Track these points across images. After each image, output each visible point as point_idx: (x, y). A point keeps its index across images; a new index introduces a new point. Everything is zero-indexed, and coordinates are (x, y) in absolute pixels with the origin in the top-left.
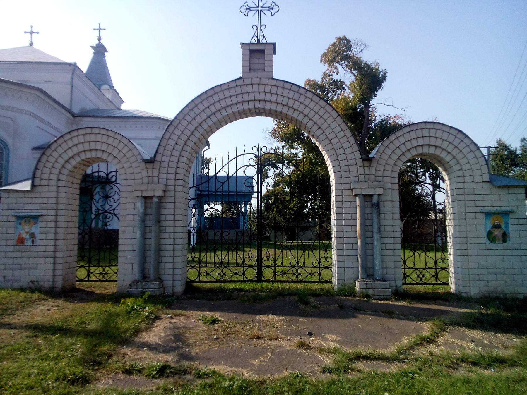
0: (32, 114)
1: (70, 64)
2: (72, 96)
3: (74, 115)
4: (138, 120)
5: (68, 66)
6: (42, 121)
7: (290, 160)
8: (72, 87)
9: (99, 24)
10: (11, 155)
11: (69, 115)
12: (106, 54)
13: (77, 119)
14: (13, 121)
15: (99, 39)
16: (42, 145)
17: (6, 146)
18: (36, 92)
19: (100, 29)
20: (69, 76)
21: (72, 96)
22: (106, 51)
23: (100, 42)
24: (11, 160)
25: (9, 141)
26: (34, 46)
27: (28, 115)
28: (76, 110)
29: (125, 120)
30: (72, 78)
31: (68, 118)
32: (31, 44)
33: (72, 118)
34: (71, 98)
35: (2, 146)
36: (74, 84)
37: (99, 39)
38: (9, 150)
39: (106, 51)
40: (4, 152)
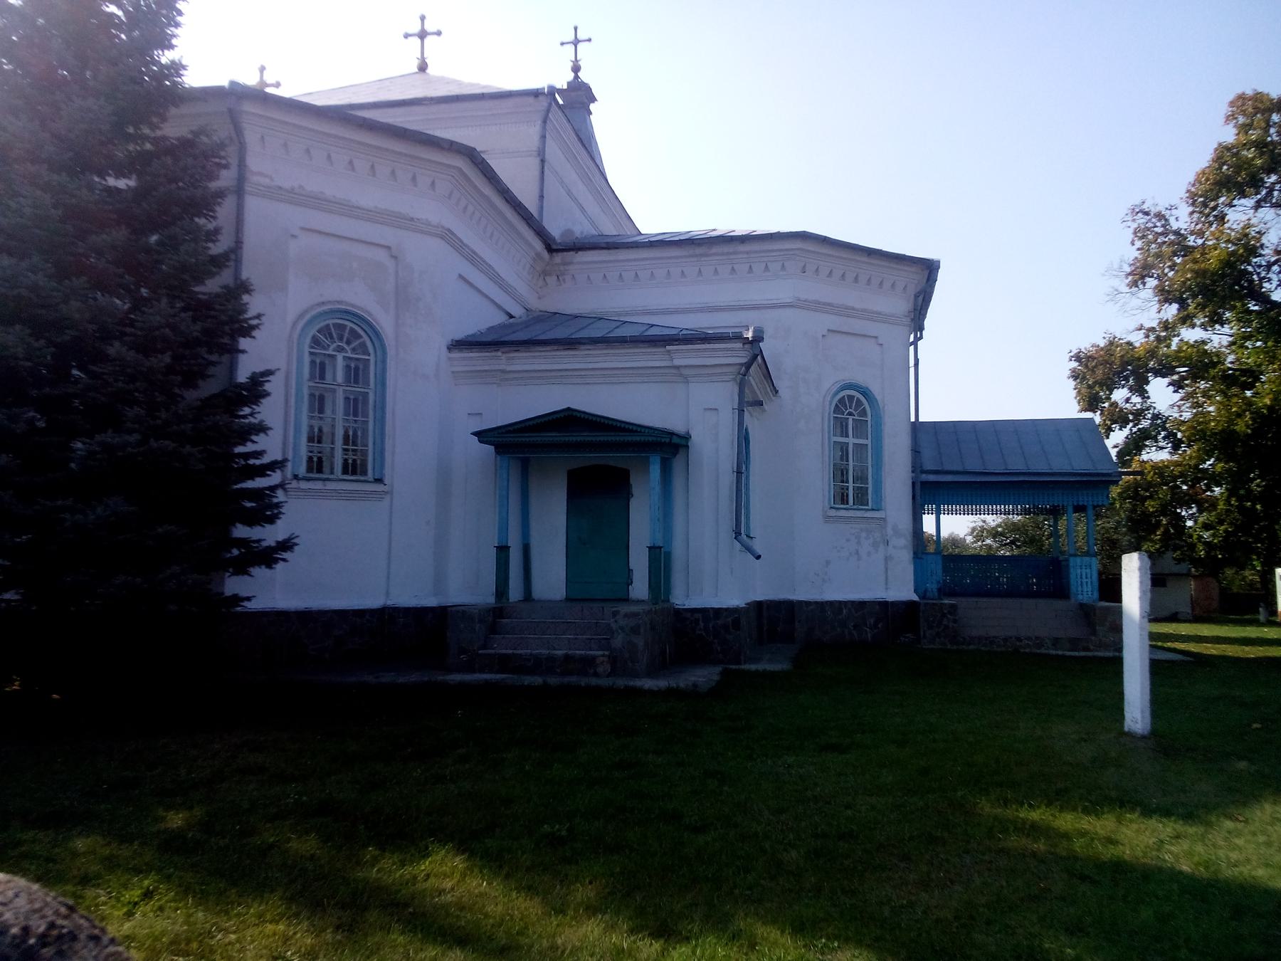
0: (448, 236)
1: (536, 94)
2: (542, 190)
3: (552, 247)
4: (742, 248)
5: (531, 100)
6: (473, 258)
7: (1200, 365)
8: (543, 161)
9: (576, 29)
10: (391, 363)
11: (538, 245)
12: (592, 107)
13: (558, 258)
14: (395, 258)
15: (576, 69)
16: (473, 335)
17: (376, 334)
18: (460, 162)
19: (576, 42)
20: (534, 131)
21: (542, 190)
22: (593, 99)
23: (577, 77)
24: (390, 382)
25: (385, 322)
26: (428, 71)
27: (436, 235)
28: (555, 229)
29: (699, 251)
30: (543, 137)
31: (538, 255)
32: (423, 67)
33: (546, 254)
34: (542, 197)
35: (365, 338)
36: (547, 157)
37: (576, 69)
38: (384, 353)
39: (593, 99)
40: (372, 358)
